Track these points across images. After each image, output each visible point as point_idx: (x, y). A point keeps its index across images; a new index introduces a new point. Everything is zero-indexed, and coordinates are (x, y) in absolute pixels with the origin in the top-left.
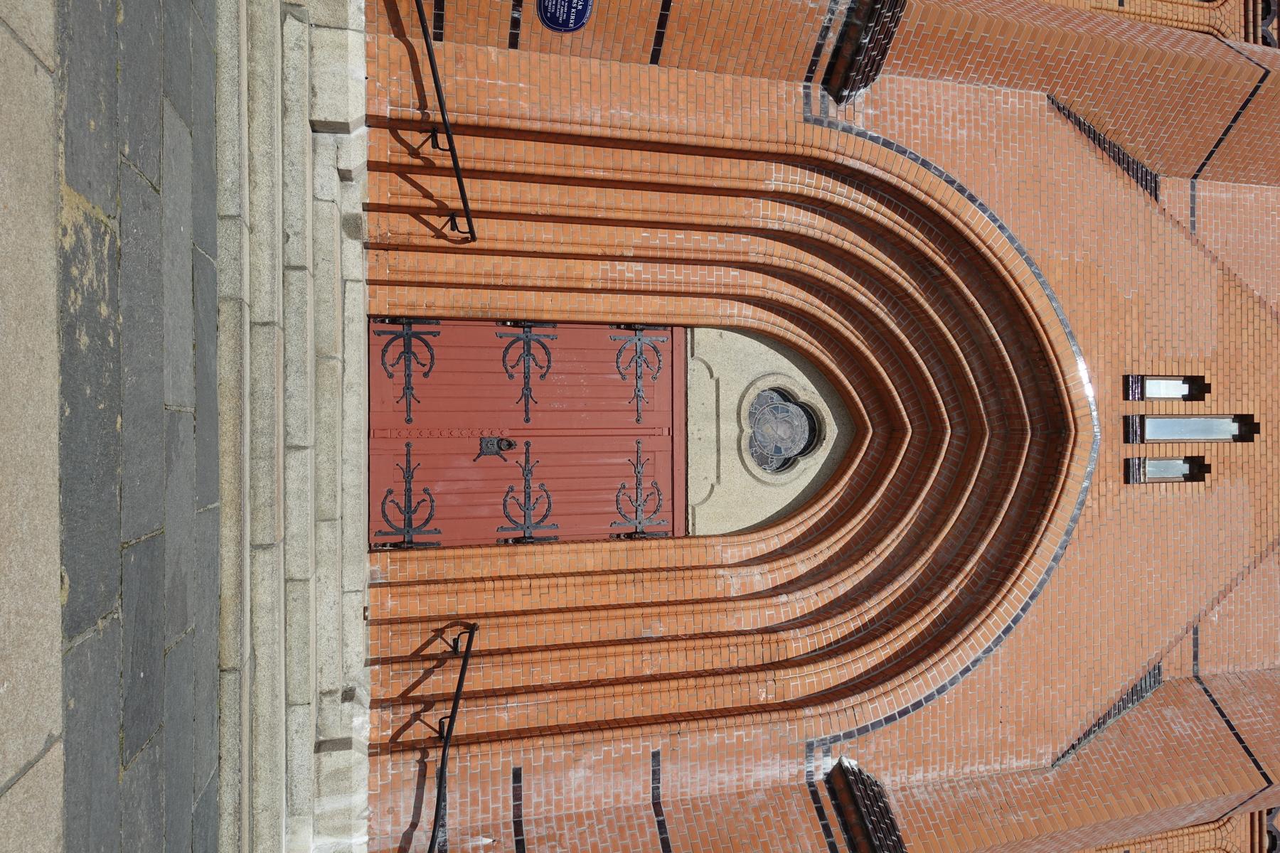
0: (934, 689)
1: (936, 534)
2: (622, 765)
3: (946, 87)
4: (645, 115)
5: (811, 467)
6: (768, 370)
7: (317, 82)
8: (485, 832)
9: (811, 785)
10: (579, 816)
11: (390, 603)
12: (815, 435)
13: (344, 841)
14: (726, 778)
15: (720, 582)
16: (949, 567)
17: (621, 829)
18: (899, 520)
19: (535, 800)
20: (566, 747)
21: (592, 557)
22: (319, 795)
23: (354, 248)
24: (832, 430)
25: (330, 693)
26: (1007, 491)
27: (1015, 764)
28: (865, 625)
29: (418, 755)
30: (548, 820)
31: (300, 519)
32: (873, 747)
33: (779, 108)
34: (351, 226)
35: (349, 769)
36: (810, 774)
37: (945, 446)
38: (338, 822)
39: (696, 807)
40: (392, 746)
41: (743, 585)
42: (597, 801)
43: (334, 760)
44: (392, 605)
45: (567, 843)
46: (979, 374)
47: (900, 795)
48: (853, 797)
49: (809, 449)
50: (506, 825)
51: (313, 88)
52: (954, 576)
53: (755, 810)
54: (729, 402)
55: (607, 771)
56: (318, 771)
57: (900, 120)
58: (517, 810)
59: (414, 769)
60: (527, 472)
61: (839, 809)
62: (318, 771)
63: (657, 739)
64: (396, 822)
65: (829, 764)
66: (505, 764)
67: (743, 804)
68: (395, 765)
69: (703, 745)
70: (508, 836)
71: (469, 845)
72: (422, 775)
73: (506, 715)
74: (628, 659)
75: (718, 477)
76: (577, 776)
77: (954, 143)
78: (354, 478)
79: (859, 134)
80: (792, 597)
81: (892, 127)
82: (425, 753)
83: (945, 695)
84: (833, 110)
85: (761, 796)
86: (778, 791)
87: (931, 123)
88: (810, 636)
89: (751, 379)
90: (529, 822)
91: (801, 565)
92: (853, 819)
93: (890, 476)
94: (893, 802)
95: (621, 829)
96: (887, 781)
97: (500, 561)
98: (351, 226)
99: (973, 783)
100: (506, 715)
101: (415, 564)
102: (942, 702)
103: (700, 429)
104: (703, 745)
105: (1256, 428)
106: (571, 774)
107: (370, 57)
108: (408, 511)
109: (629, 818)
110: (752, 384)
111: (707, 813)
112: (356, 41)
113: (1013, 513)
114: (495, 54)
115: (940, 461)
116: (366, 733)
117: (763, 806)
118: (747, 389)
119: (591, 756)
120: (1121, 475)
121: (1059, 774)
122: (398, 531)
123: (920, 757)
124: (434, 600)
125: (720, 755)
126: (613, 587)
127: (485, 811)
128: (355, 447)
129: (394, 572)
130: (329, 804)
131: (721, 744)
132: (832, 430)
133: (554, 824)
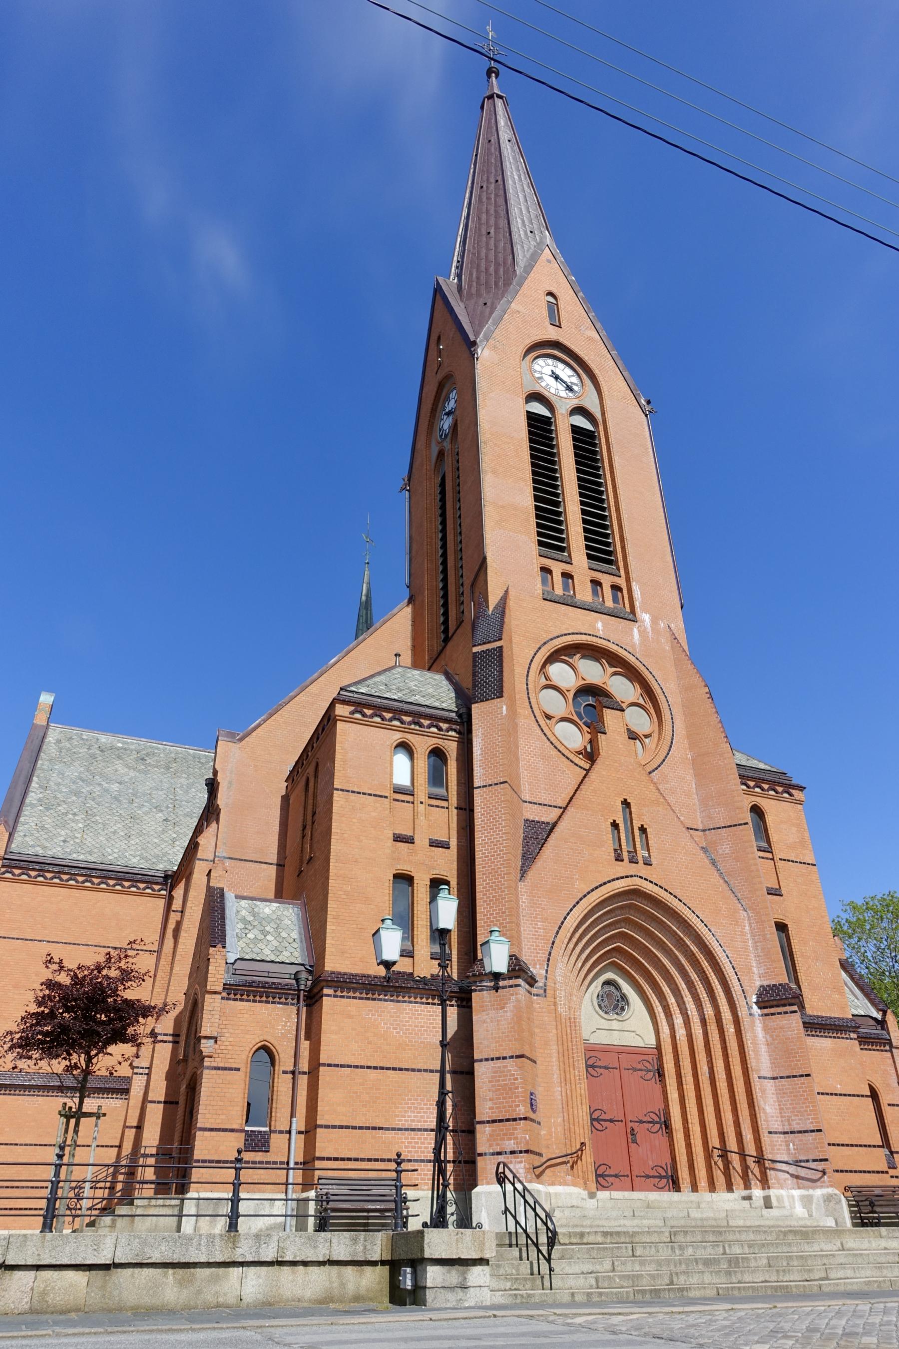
0: (728, 960)
1: (664, 942)
2: (763, 1091)
3: (524, 930)
4: (555, 1068)
5: (627, 988)
6: (590, 1004)
7: (569, 1205)
8: (788, 1145)
9: (762, 1015)
10: (780, 1109)
11: (703, 1184)
13: (796, 1198)
14: (763, 1050)
15: (682, 1039)
16: (678, 940)
17: (784, 1093)
18: (656, 956)
19: (776, 1126)
20: (760, 1113)
22: (784, 1207)
24: (610, 975)
25: (750, 1204)
26: (653, 914)
27: (747, 928)
28: (700, 980)
29: (768, 1171)
30: (782, 1121)
32: (748, 988)
33: (543, 1008)
35: (776, 1196)
36: (759, 1015)
37: (629, 932)
38: (791, 1200)
39: (774, 1063)
40: (765, 1183)
41: (681, 1028)
42: (774, 1101)
43: (774, 1202)
44: (703, 1183)
45: (790, 1114)
46: (608, 917)
47: (762, 979)
48: (767, 1001)
49: (618, 987)
50: (785, 1137)
51: (572, 1207)
52: (684, 941)
53: (773, 1040)
54: (604, 1024)
55: (766, 1097)
56: (778, 1207)
57: (539, 953)
58: (780, 1133)
59: (772, 1172)
60: (641, 1122)
61: (772, 1007)
62: (778, 1207)
63: (754, 1077)
64: (788, 1179)
65: (755, 1007)
66: (768, 1137)
67: (771, 1044)
68: (771, 1179)
69: (754, 1058)
70: (789, 1137)
71: (793, 1152)
72: (773, 1169)
73: (748, 1136)
74: (721, 1084)
75: (633, 1032)
77: (544, 929)
79: (547, 973)
80: (689, 1009)
81: (542, 957)
82: (767, 1168)
83: (729, 955)
84: (540, 984)
85: (768, 1037)
86: (766, 1029)
87: (538, 939)
88: (706, 1005)
89: (595, 1013)
90: (784, 1129)
92: (775, 1003)
93: (636, 955)
94: (766, 983)
95: (784, 1093)
96: (758, 984)
97: (679, 1136)
99: (756, 948)
100: (748, 1136)
102: (732, 957)
103: (615, 1039)
104: (754, 1058)
106: (768, 1111)
107: (553, 1184)
109: (780, 1090)
110: (597, 1013)
111: (776, 1059)
113: (661, 913)
115: (635, 935)
116: (759, 1191)
117: (772, 1036)
118: (599, 1015)
119: (762, 1103)
120: (649, 867)
121: (750, 910)
122: (668, 1182)
124: (700, 1165)
126: (688, 1087)
127: (781, 1145)
129: (687, 1183)
130: (787, 1204)
131: (753, 1051)
132: (610, 975)
133: (783, 1119)
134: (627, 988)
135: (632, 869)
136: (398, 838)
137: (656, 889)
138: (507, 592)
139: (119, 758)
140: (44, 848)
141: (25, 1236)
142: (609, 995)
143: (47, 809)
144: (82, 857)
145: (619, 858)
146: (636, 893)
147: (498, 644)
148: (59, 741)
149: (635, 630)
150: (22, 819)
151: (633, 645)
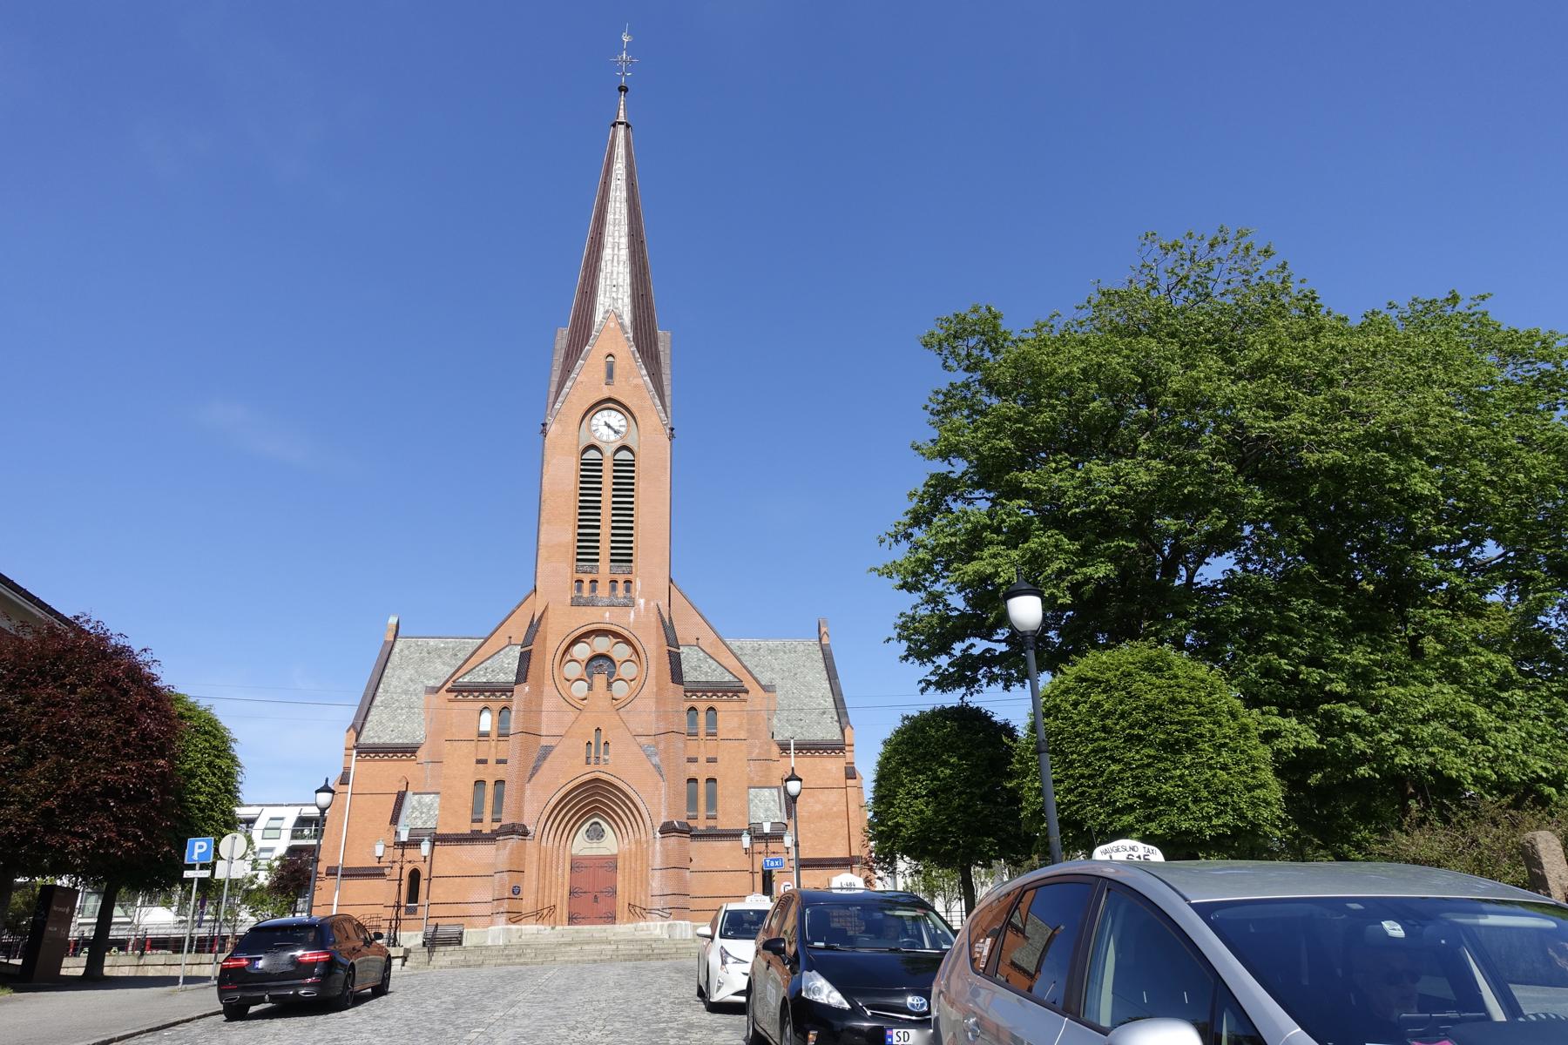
2: (653, 876)
5: (604, 825)
12: (597, 823)
21: (620, 878)
23: (557, 928)
24: (596, 820)
31: (605, 934)
34: (553, 928)
54: (588, 845)
65: (658, 834)
76: (654, 885)
78: (599, 927)
86: (662, 845)
91: (624, 831)
98: (553, 928)
101: (619, 916)
103: (594, 852)
105: (598, 729)
108: (608, 917)
112: (523, 927)
114: (524, 902)
123: (659, 814)
125: (653, 857)
128: (594, 927)
132: (596, 820)
134: (604, 825)
135: (596, 768)
136: (479, 762)
137: (609, 777)
138: (547, 607)
139: (440, 656)
140: (379, 738)
141: (515, 917)
142: (595, 830)
143: (386, 708)
144: (401, 741)
145: (588, 763)
146: (597, 780)
147: (530, 647)
148: (402, 650)
149: (632, 613)
150: (369, 718)
151: (629, 624)
